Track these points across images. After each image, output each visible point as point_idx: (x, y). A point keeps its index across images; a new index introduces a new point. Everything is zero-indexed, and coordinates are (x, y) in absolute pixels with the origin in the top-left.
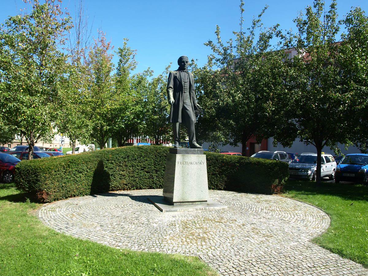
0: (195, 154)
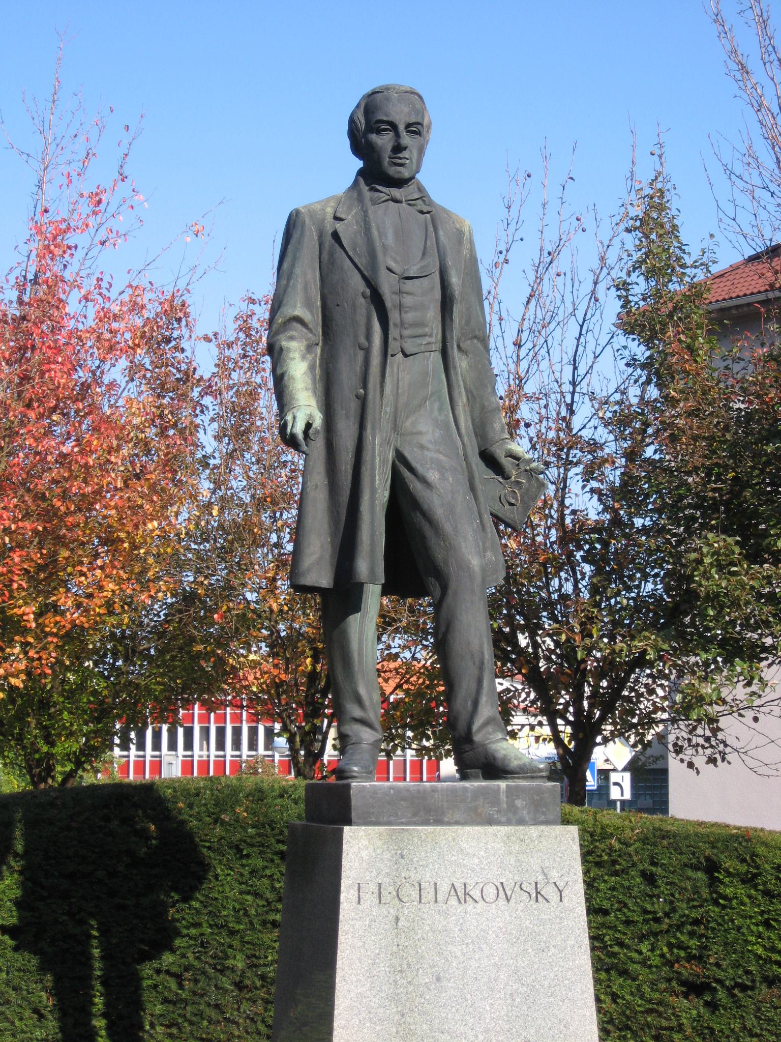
0: (490, 822)
